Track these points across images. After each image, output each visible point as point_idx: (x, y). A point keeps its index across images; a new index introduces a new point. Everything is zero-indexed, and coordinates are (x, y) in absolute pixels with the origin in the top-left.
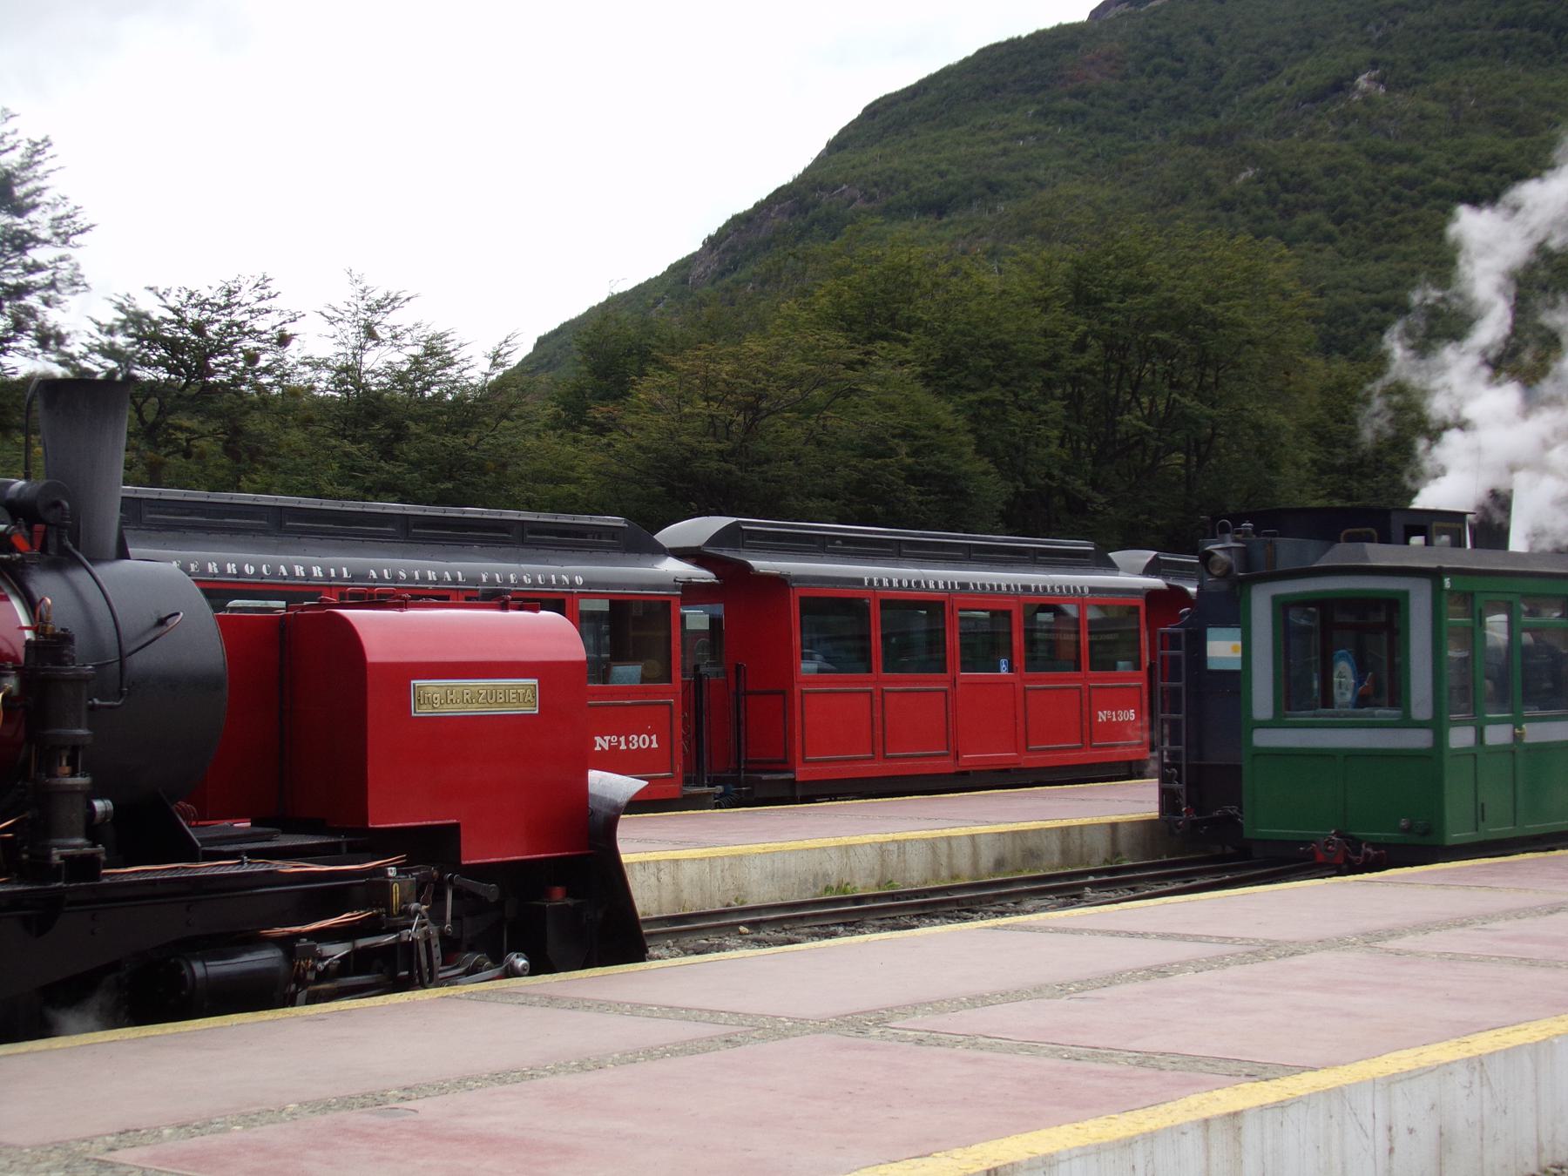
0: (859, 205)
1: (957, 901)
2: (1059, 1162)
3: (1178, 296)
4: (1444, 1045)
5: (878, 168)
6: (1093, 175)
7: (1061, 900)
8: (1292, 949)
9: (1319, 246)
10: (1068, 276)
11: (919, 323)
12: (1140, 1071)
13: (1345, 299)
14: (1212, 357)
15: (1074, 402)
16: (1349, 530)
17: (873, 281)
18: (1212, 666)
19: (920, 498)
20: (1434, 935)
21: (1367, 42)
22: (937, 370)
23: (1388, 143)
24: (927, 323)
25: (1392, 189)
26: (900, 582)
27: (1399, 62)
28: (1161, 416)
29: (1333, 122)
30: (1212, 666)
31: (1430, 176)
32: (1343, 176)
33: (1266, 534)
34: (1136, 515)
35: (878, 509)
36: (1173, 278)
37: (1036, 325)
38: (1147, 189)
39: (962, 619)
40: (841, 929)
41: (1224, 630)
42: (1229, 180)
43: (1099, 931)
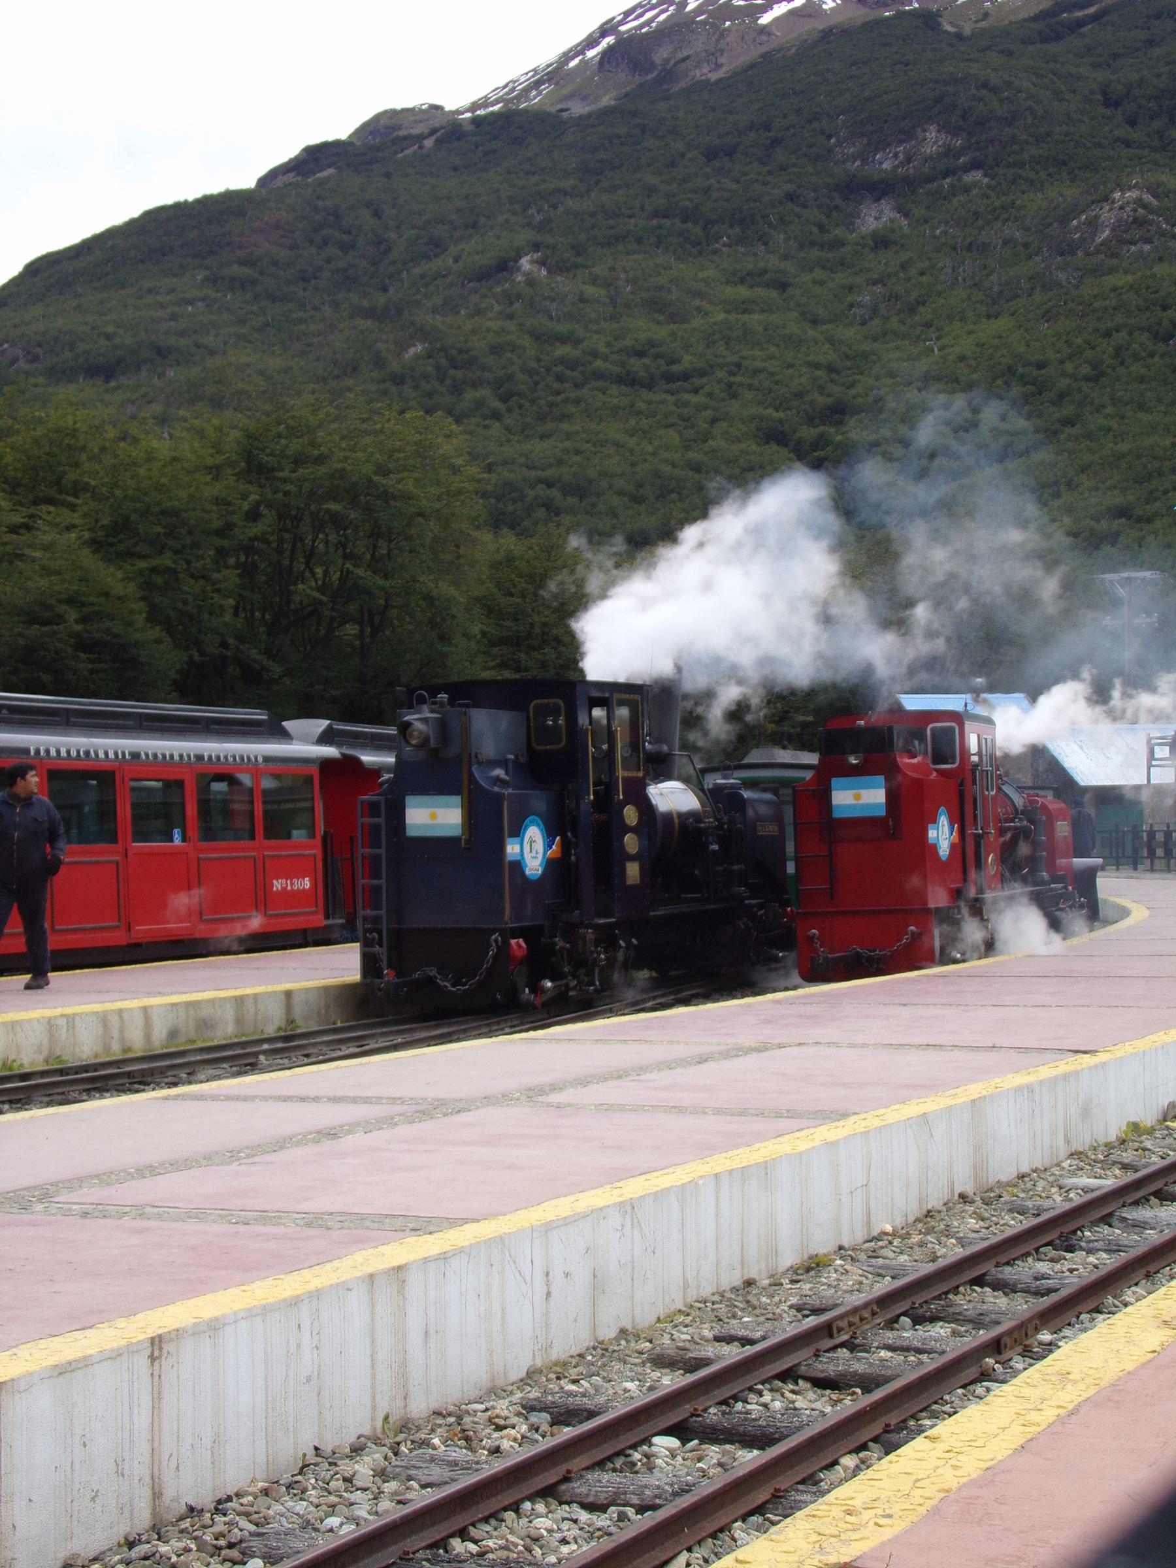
0: (22, 364)
1: (129, 1075)
2: (224, 1325)
4: (599, 1191)
5: (41, 327)
7: (234, 1069)
8: (459, 1107)
9: (487, 422)
11: (86, 488)
12: (309, 1232)
15: (248, 572)
16: (538, 701)
17: (36, 442)
19: (90, 666)
20: (593, 1088)
21: (529, 224)
22: (107, 536)
23: (550, 324)
24: (95, 488)
26: (68, 752)
28: (335, 586)
31: (590, 358)
35: (46, 678)
37: (208, 492)
38: (318, 360)
39: (133, 789)
40: (6, 1107)
42: (399, 354)
43: (271, 1098)
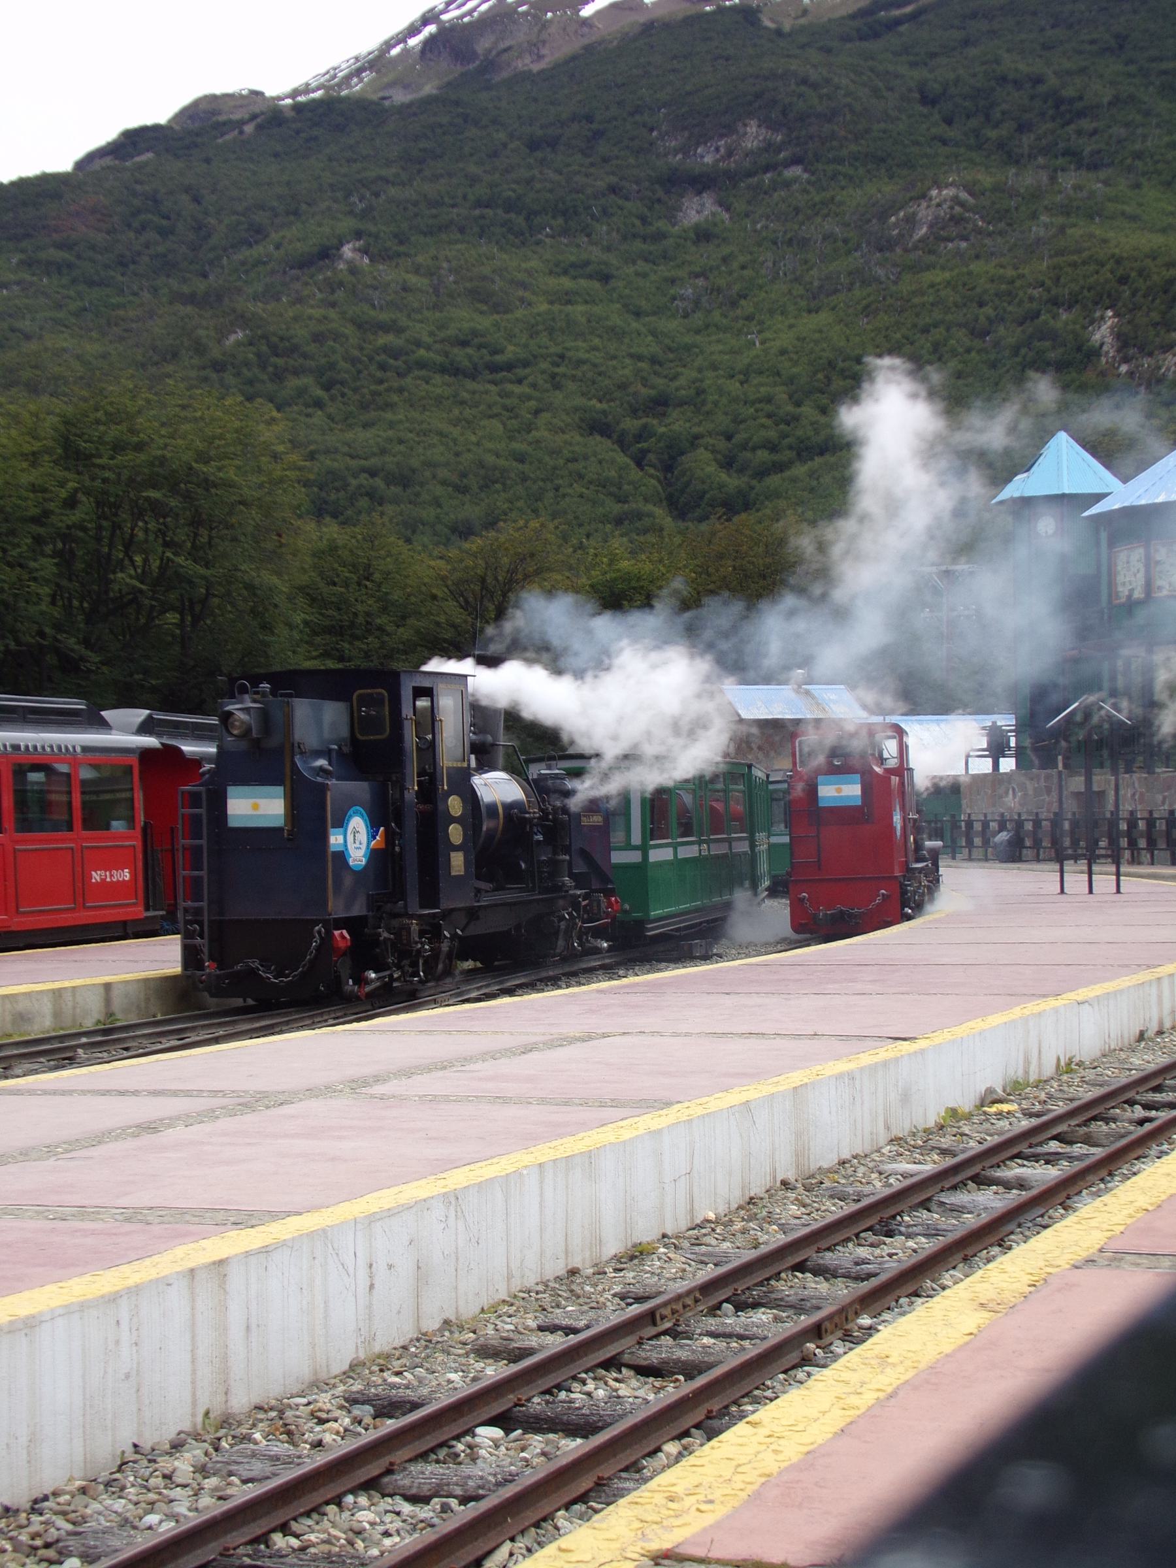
3: (169, 455)
4: (423, 1182)
6: (81, 329)
9: (310, 410)
10: (56, 430)
12: (128, 1227)
13: (336, 464)
14: (204, 517)
15: (65, 559)
18: (232, 823)
20: (417, 1079)
23: (372, 313)
25: (378, 358)
27: (382, 234)
28: (155, 575)
29: (320, 290)
30: (232, 823)
31: (414, 348)
32: (331, 343)
33: (282, 695)
34: (131, 675)
36: (164, 436)
37: (25, 479)
41: (246, 788)
42: (219, 342)
43: (89, 1091)
